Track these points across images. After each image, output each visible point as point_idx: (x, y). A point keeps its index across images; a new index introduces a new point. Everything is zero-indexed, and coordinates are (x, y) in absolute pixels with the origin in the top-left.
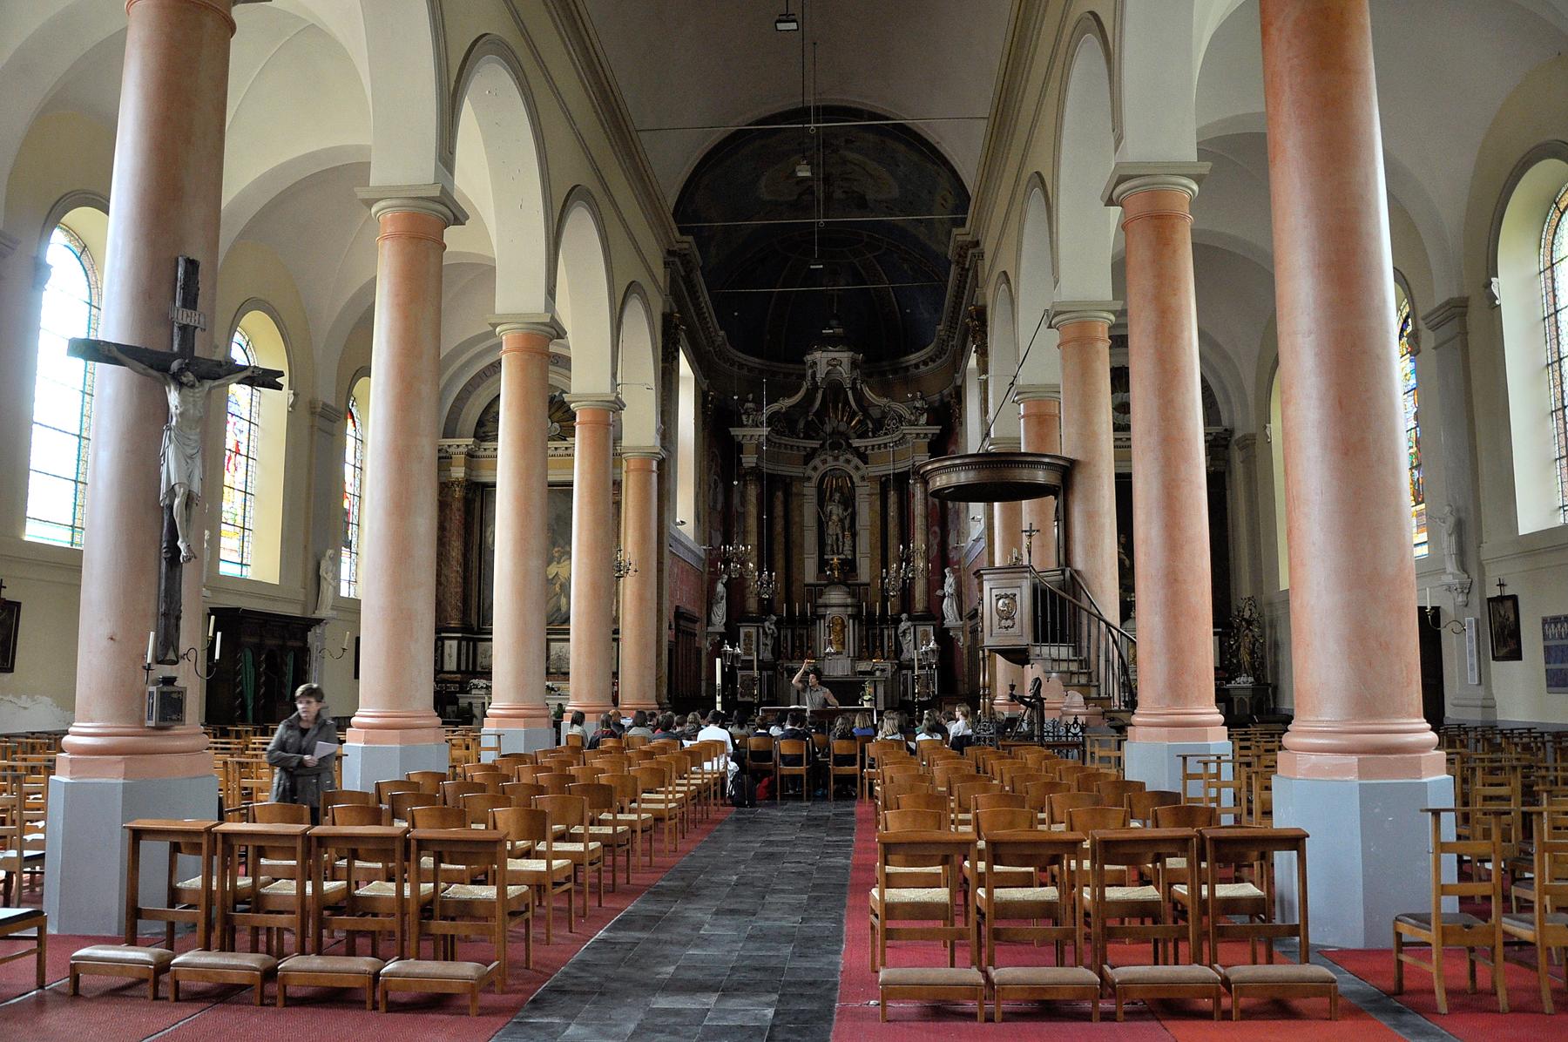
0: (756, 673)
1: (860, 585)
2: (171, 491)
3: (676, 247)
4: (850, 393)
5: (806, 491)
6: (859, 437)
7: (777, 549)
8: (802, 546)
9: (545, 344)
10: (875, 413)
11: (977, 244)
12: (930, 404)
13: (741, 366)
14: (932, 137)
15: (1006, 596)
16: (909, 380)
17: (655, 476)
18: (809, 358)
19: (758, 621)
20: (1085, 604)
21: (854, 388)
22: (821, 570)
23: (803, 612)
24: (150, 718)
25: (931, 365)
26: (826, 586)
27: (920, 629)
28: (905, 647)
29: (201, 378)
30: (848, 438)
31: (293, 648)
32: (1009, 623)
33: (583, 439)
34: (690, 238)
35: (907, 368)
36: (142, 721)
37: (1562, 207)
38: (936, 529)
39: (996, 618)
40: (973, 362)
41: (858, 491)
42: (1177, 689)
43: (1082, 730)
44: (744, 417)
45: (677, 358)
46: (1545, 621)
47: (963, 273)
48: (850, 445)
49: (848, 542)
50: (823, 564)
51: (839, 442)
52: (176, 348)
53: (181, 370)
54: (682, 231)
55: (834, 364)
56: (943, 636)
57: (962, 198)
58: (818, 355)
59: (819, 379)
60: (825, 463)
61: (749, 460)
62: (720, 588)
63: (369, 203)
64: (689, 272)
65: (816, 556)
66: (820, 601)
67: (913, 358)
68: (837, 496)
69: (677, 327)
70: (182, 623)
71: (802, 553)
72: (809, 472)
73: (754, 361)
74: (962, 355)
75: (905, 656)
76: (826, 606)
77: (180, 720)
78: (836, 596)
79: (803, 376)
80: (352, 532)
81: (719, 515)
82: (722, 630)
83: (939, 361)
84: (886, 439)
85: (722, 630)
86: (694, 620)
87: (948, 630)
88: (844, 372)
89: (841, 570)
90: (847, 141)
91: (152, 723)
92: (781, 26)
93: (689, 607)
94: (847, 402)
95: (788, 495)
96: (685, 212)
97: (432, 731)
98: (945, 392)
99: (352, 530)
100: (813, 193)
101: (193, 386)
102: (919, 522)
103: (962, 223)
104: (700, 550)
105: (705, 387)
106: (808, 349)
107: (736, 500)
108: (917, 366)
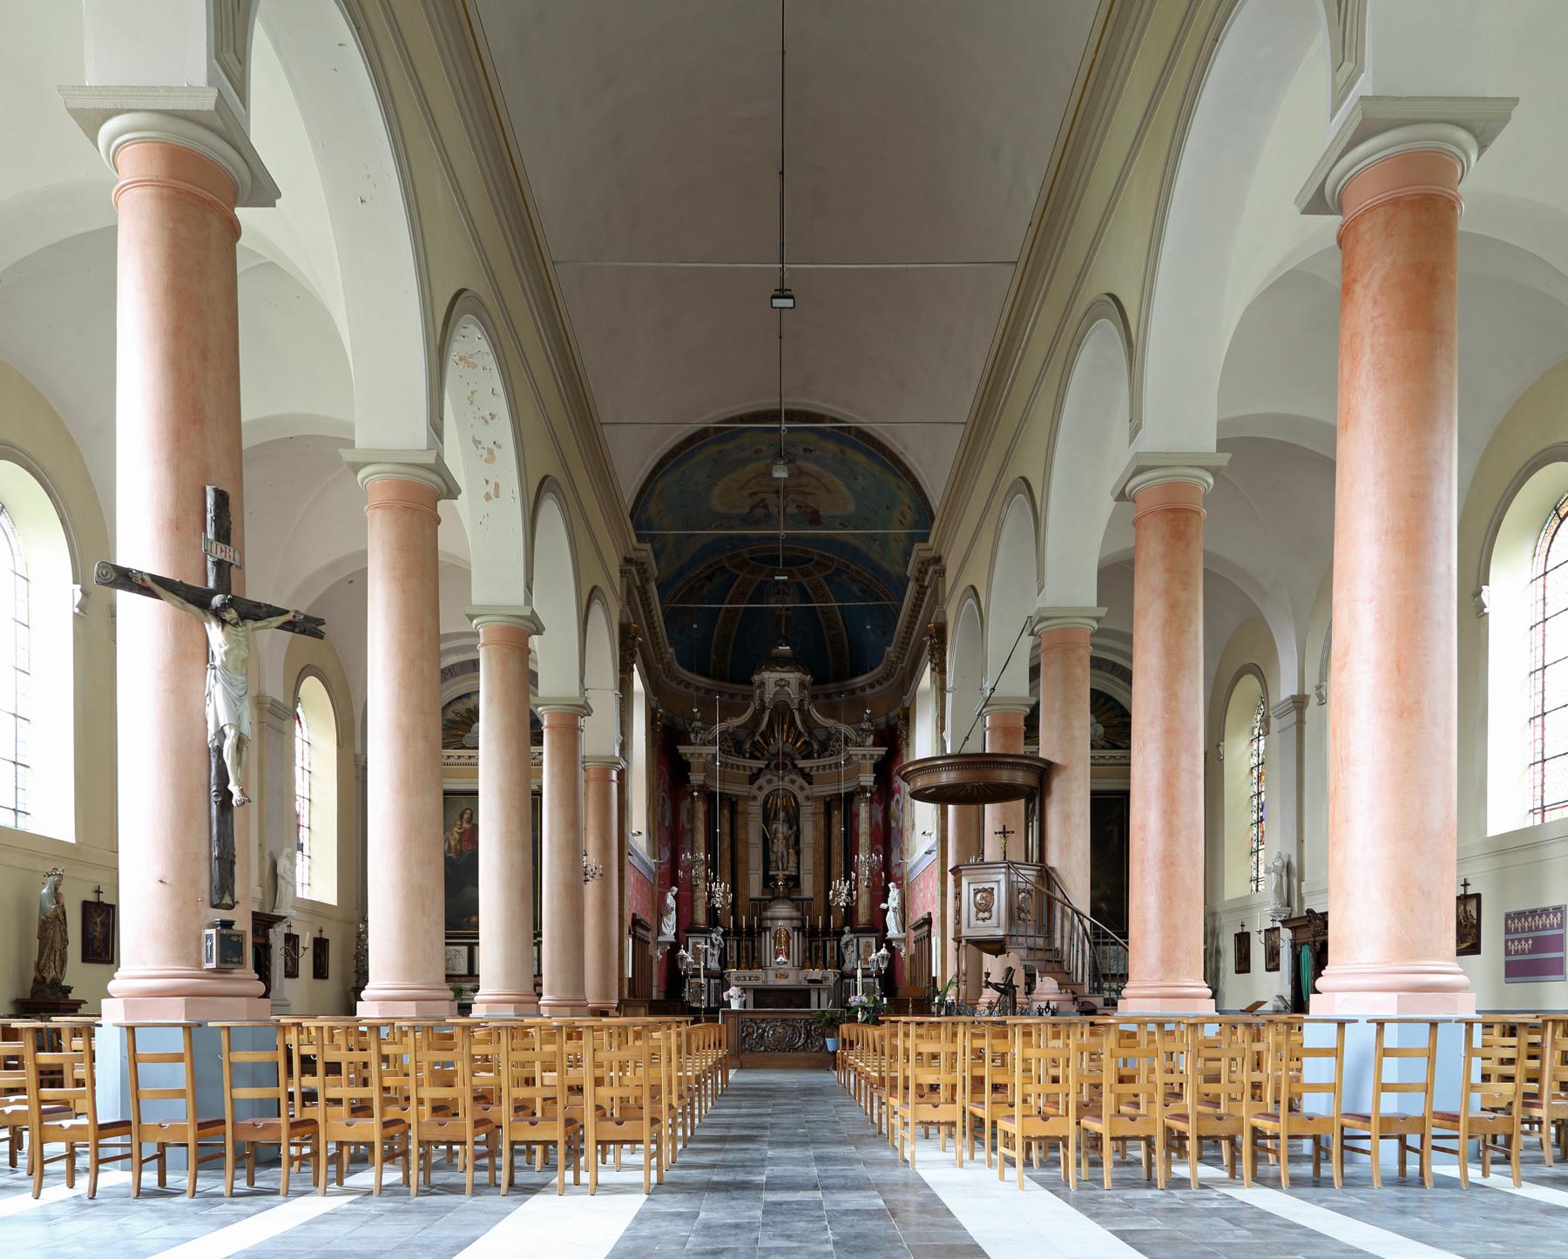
0: (703, 981)
2: (221, 733)
3: (633, 555)
4: (797, 715)
5: (751, 809)
6: (804, 758)
8: (747, 862)
9: (520, 634)
10: (821, 734)
11: (938, 560)
13: (698, 689)
14: (896, 446)
15: (984, 890)
16: (853, 708)
17: (614, 786)
18: (756, 678)
19: (705, 932)
20: (1059, 895)
21: (800, 709)
24: (209, 960)
25: (878, 688)
27: (863, 941)
28: (847, 958)
29: (243, 617)
30: (793, 759)
32: (987, 915)
35: (853, 691)
36: (199, 965)
37: (1562, 514)
38: (880, 847)
39: (973, 910)
40: (926, 681)
41: (802, 811)
42: (1168, 962)
46: (1508, 917)
47: (922, 591)
48: (795, 766)
49: (793, 859)
50: (768, 880)
51: (784, 763)
52: (211, 584)
53: (224, 606)
54: (640, 539)
55: (783, 684)
57: (924, 516)
58: (766, 675)
60: (766, 785)
61: (696, 778)
62: (670, 901)
63: (356, 467)
64: (645, 580)
66: (769, 914)
67: (860, 680)
68: (782, 815)
69: (634, 638)
70: (237, 868)
71: (747, 869)
73: (703, 681)
74: (913, 674)
76: (772, 919)
77: (241, 963)
78: (782, 910)
79: (748, 697)
80: (304, 835)
81: (670, 831)
83: (886, 684)
84: (832, 760)
88: (793, 692)
89: (786, 885)
90: (805, 450)
91: (213, 965)
92: (778, 303)
94: (792, 723)
95: (733, 814)
96: (640, 517)
98: (892, 714)
99: (304, 833)
100: (766, 507)
102: (864, 840)
103: (925, 538)
104: (651, 862)
105: (654, 704)
106: (756, 667)
107: (684, 817)
108: (863, 689)
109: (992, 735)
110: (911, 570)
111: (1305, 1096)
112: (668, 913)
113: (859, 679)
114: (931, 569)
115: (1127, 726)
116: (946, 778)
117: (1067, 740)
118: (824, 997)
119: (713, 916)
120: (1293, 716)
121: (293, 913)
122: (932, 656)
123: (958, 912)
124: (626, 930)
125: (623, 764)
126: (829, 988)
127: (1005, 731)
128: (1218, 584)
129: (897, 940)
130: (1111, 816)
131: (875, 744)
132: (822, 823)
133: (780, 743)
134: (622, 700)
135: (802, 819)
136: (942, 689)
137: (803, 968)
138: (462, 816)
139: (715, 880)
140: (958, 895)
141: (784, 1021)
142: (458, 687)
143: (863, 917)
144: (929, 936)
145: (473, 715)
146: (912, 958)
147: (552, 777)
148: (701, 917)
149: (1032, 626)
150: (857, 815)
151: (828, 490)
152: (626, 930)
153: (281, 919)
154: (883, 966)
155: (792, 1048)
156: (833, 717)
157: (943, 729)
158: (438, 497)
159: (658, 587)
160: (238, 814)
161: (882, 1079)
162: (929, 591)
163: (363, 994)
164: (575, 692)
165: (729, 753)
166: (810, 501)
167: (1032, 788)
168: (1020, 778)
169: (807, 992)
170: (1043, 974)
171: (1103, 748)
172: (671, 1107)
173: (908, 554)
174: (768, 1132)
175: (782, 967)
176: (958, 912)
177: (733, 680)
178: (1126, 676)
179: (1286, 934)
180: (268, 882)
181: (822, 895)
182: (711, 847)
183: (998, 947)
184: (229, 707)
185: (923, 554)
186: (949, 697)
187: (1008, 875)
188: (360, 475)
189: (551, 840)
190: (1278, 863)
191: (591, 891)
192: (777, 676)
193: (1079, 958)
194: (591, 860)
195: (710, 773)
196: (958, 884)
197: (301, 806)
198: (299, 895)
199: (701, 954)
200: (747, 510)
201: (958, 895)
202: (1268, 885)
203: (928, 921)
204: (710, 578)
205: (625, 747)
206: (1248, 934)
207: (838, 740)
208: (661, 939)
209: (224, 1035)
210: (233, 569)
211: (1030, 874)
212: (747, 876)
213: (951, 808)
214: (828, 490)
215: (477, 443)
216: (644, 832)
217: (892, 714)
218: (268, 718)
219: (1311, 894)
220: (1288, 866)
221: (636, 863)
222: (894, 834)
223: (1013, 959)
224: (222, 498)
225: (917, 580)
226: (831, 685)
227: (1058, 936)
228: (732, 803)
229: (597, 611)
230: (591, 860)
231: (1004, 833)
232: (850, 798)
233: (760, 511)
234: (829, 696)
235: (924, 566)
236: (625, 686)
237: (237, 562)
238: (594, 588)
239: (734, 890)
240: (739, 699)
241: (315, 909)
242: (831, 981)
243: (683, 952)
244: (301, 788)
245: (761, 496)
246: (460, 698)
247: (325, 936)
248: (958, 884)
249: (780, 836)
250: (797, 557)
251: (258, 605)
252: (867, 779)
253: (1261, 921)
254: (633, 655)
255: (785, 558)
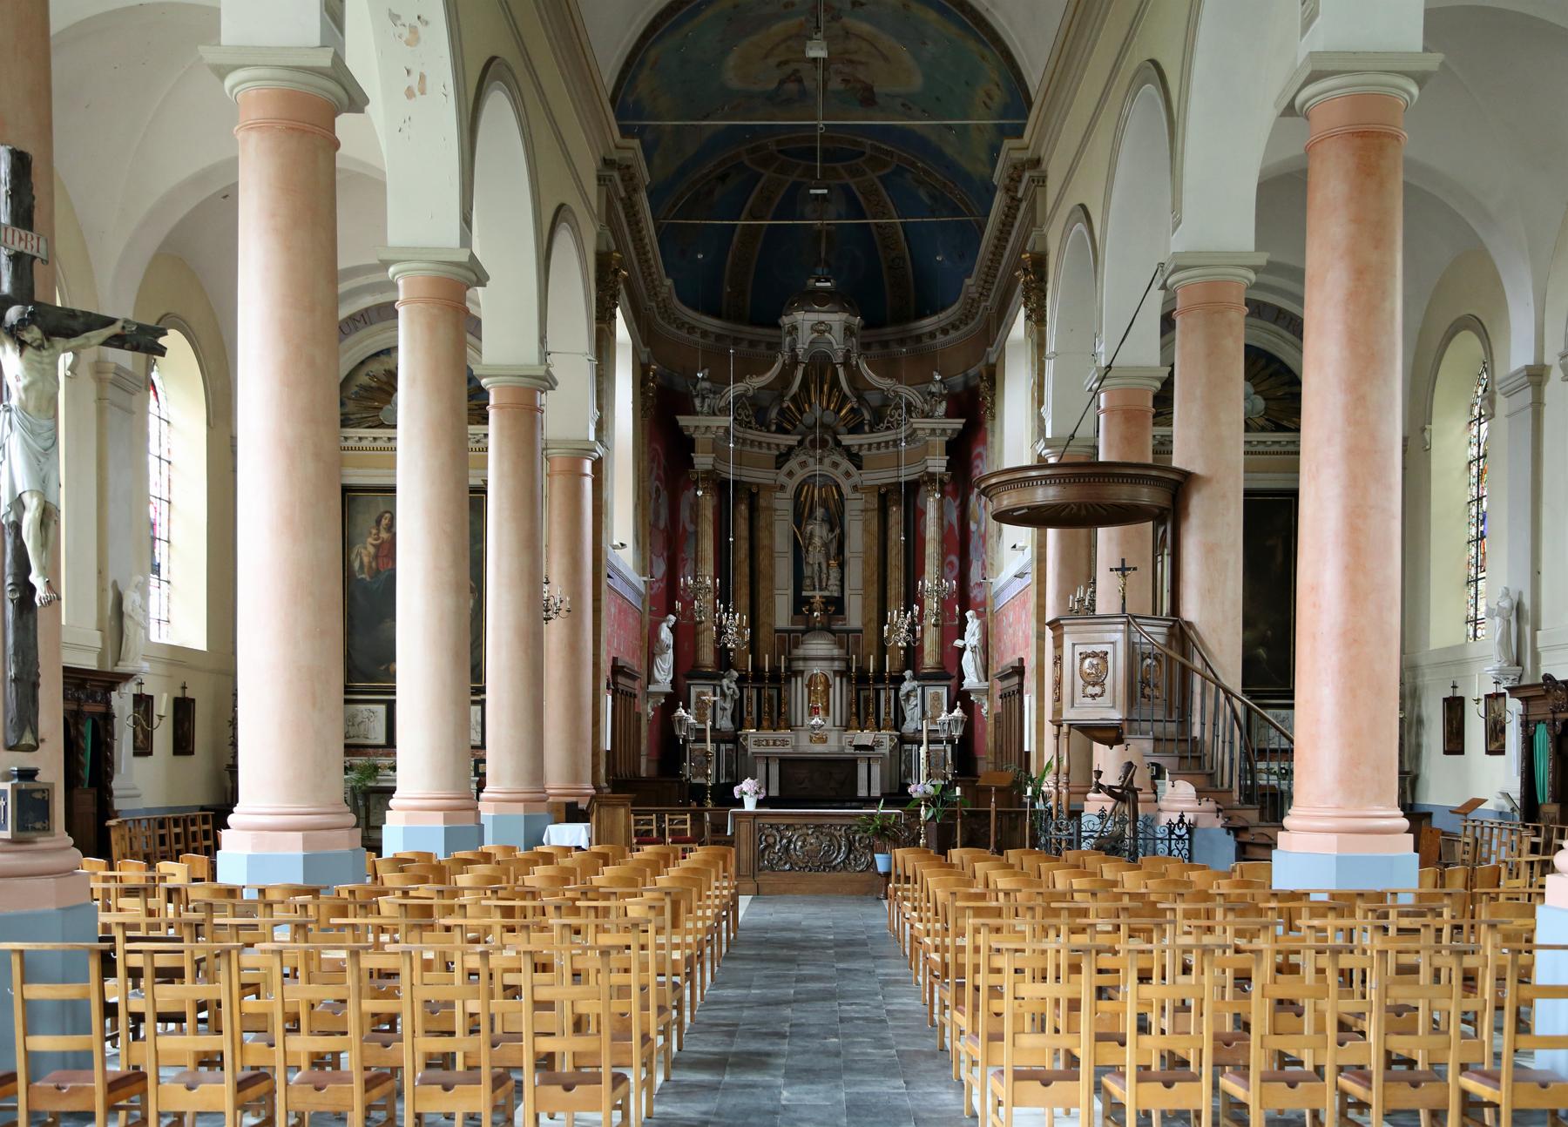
0: (709, 747)
1: (848, 632)
2: (18, 504)
3: (616, 156)
5: (778, 504)
6: (852, 431)
7: (741, 580)
8: (772, 579)
9: (456, 293)
11: (1036, 163)
12: (951, 388)
13: (705, 334)
15: (1094, 655)
16: (922, 360)
17: (588, 483)
18: (786, 320)
19: (713, 678)
22: (797, 610)
23: (775, 670)
26: (804, 633)
27: (930, 691)
28: (908, 714)
30: (835, 433)
31: (92, 714)
32: (1097, 690)
33: (500, 429)
34: (636, 143)
35: (919, 338)
38: (954, 559)
39: (1079, 682)
40: (1019, 328)
41: (848, 506)
43: (1189, 831)
44: (697, 402)
45: (614, 316)
48: (838, 443)
49: (834, 573)
50: (800, 603)
51: (825, 439)
53: (22, 323)
54: (626, 132)
55: (820, 329)
56: (961, 697)
57: (1018, 100)
58: (800, 316)
59: (800, 352)
61: (703, 460)
62: (666, 635)
63: (222, 72)
64: (632, 189)
65: (790, 592)
66: (800, 652)
67: (928, 323)
68: (819, 512)
69: (616, 272)
72: (782, 478)
73: (711, 324)
75: (909, 727)
76: (805, 659)
77: (47, 829)
79: (775, 346)
81: (664, 535)
82: (668, 689)
83: (964, 329)
84: (889, 436)
85: (668, 689)
86: (632, 676)
87: (967, 693)
88: (836, 342)
89: (825, 611)
93: (626, 660)
94: (835, 383)
95: (753, 510)
96: (626, 103)
97: (345, 832)
98: (971, 372)
100: (800, 81)
101: (40, 348)
102: (931, 549)
103: (1018, 132)
104: (638, 580)
105: (644, 358)
107: (685, 514)
108: (932, 335)
109: (1108, 421)
110: (999, 176)
111: (1539, 1004)
112: (663, 652)
113: (926, 322)
114: (1027, 175)
115: (1296, 397)
116: (1043, 495)
117: (1208, 437)
118: (876, 770)
119: (724, 659)
120: (1527, 396)
121: (146, 666)
122: (1027, 298)
123: (1058, 684)
124: (603, 685)
125: (600, 450)
126: (882, 758)
127: (1127, 415)
128: (1425, 204)
129: (977, 691)
130: (1271, 524)
131: (948, 415)
132: (875, 523)
133: (816, 411)
134: (599, 332)
135: (847, 518)
136: (1041, 345)
137: (847, 728)
138: (378, 522)
139: (726, 610)
140: (1058, 660)
141: (816, 826)
142: (366, 342)
143: (929, 660)
144: (1020, 692)
145: (387, 387)
146: (997, 718)
147: (500, 477)
148: (707, 657)
149: (1165, 276)
150: (924, 513)
151: (886, 59)
152: (603, 685)
153: (127, 677)
154: (957, 733)
155: (828, 866)
156: (891, 377)
157: (1041, 403)
158: (333, 111)
159: (650, 196)
160: (43, 616)
161: (946, 966)
162: (1023, 206)
163: (231, 819)
164: (531, 355)
165: (748, 425)
166: (861, 74)
167: (1162, 509)
168: (1146, 496)
169: (852, 763)
170: (1175, 776)
171: (1263, 429)
172: (645, 1038)
173: (995, 150)
174: (785, 1046)
175: (819, 731)
176: (1058, 684)
177: (754, 322)
178: (1294, 325)
179: (1514, 706)
180: (110, 624)
181: (874, 625)
182: (722, 569)
183: (1113, 734)
184: (30, 466)
185: (1017, 155)
186: (1050, 366)
187: (1129, 634)
188: (229, 81)
189: (498, 567)
190: (1505, 604)
191: (555, 633)
192: (813, 317)
193: (1226, 751)
194: (556, 590)
195: (718, 449)
196: (1058, 644)
197: (157, 511)
198: (154, 638)
199: (706, 711)
200: (773, 86)
201: (1058, 660)
202: (1491, 632)
203: (1019, 671)
204: (723, 178)
205: (603, 427)
206: (1461, 700)
207: (898, 407)
208: (652, 688)
209: (16, 960)
210: (37, 264)
211: (1156, 633)
212: (772, 598)
213: (1052, 533)
214: (886, 59)
215: (395, 17)
216: (629, 540)
217: (971, 372)
218: (111, 392)
219: (1550, 648)
220: (1519, 608)
221: (617, 584)
222: (974, 541)
223: (1139, 748)
224: (21, 165)
225: (1008, 190)
226: (889, 330)
227: (1196, 719)
228: (751, 495)
229: (564, 242)
230: (556, 590)
231: (1123, 570)
232: (913, 489)
233: (792, 87)
234: (885, 344)
235: (1018, 169)
236: (604, 319)
237: (42, 254)
238: (561, 207)
239: (753, 623)
240: (762, 349)
241: (177, 657)
242: (885, 749)
243: (681, 712)
244: (156, 487)
245: (794, 66)
246: (377, 354)
247: (189, 694)
248: (1058, 644)
249: (817, 541)
250: (841, 151)
251: (72, 314)
252: (938, 464)
253: (1480, 684)
254: (614, 297)
255: (825, 151)
